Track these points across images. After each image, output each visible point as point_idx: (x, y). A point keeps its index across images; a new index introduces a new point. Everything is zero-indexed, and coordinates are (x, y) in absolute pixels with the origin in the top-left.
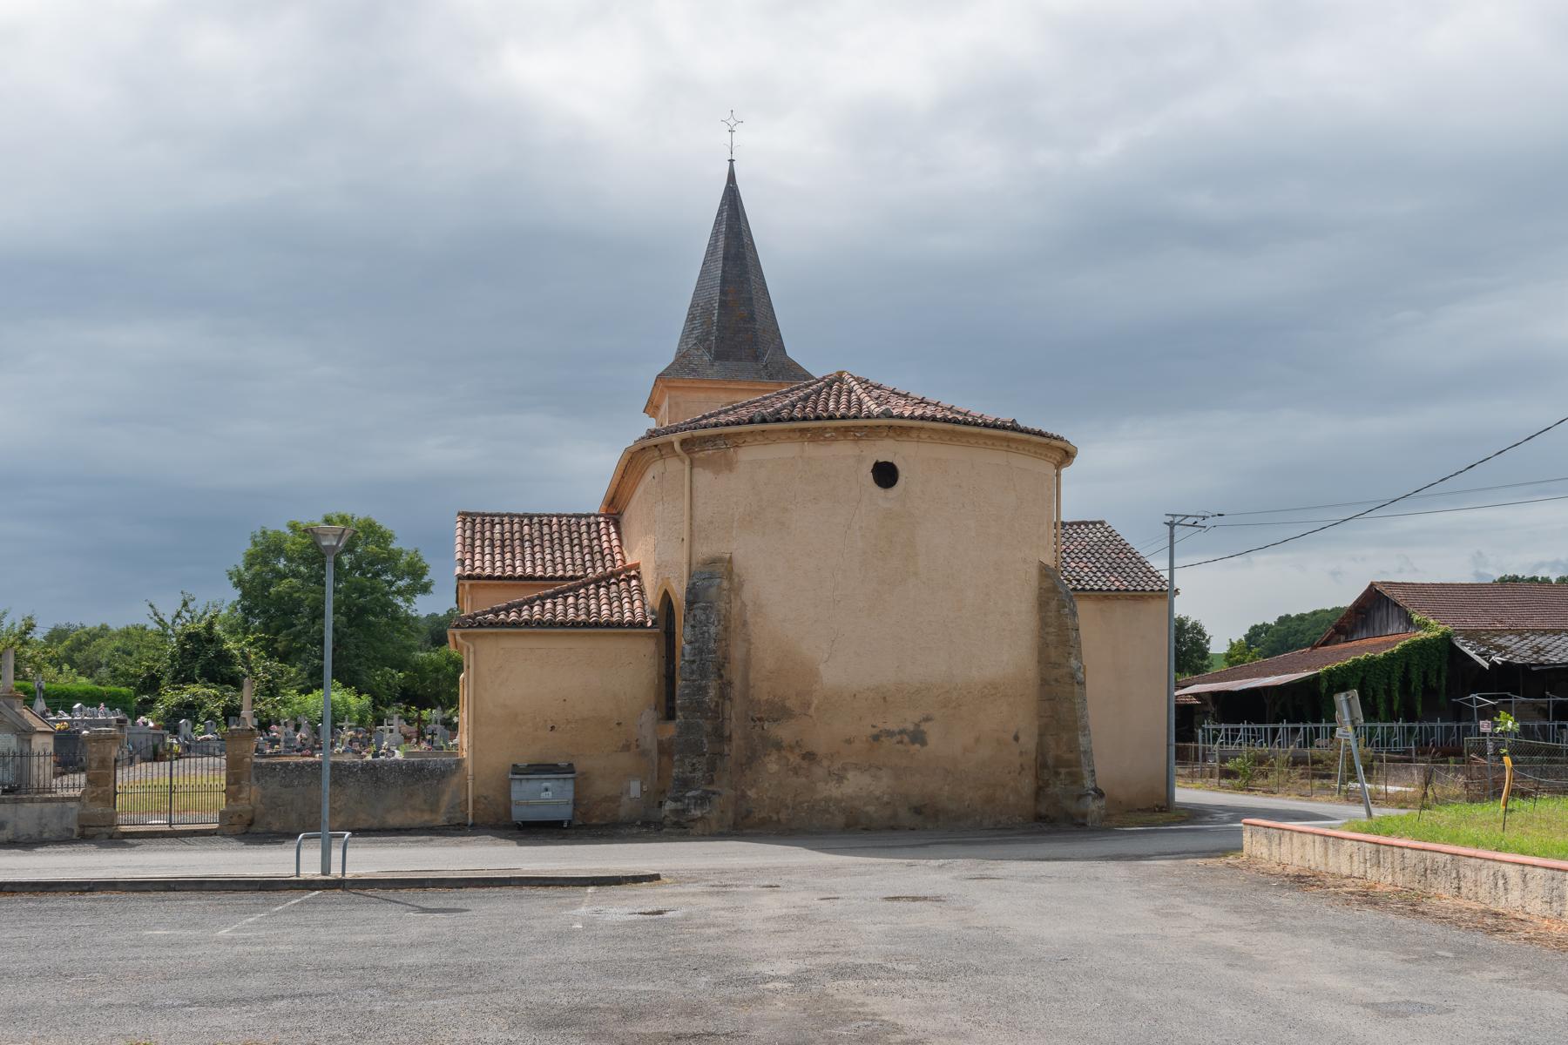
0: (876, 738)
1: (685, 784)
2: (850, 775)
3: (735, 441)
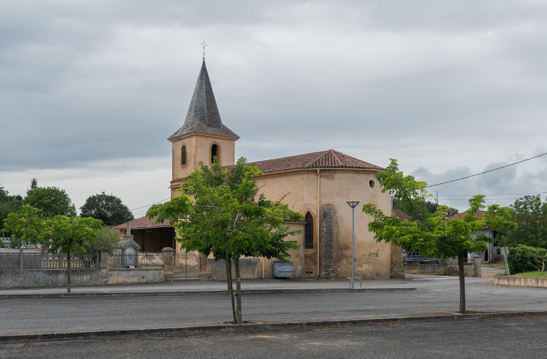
0: (370, 255)
1: (328, 267)
2: (364, 265)
3: (335, 171)
